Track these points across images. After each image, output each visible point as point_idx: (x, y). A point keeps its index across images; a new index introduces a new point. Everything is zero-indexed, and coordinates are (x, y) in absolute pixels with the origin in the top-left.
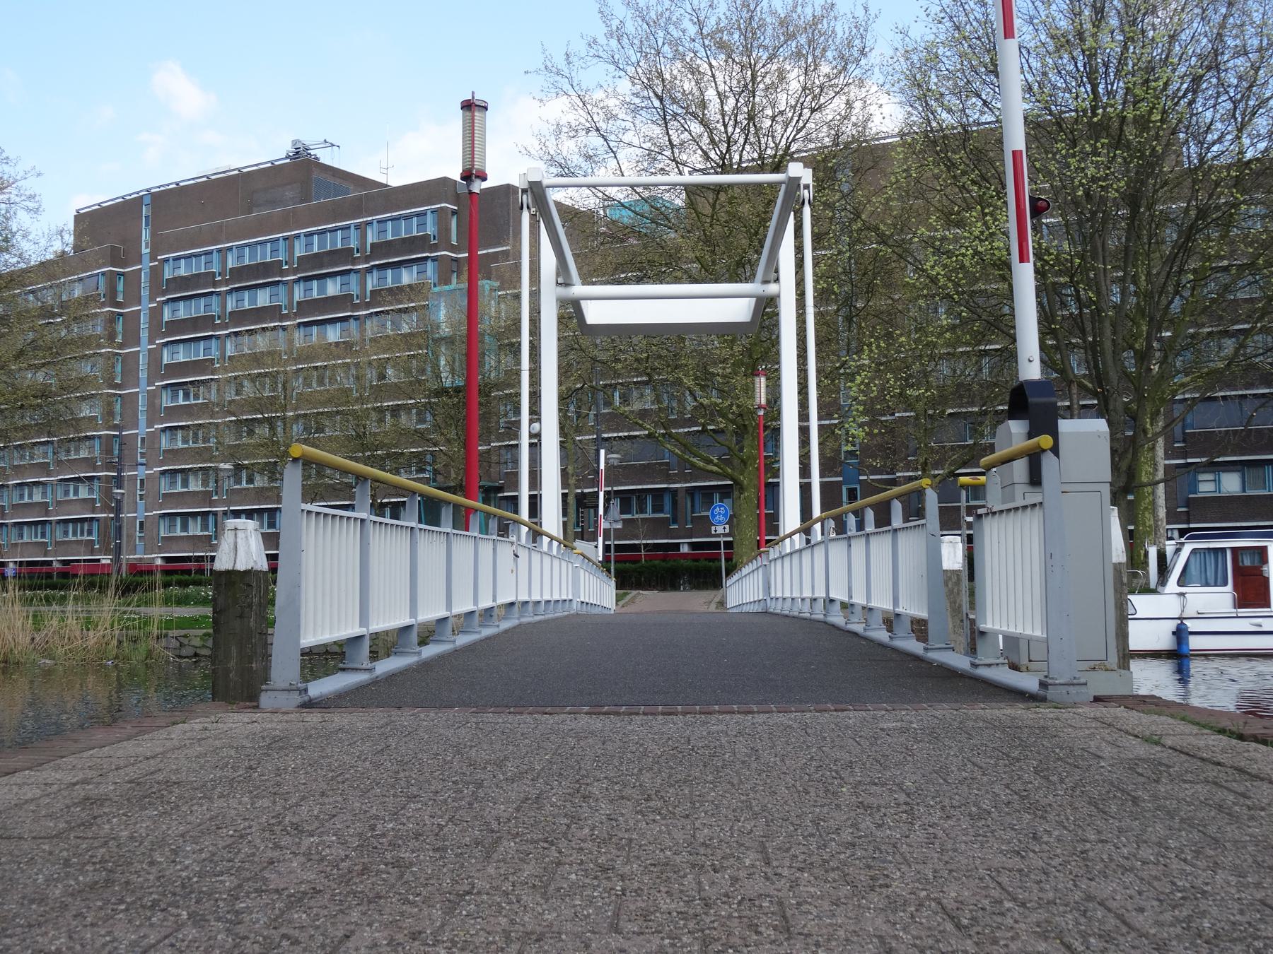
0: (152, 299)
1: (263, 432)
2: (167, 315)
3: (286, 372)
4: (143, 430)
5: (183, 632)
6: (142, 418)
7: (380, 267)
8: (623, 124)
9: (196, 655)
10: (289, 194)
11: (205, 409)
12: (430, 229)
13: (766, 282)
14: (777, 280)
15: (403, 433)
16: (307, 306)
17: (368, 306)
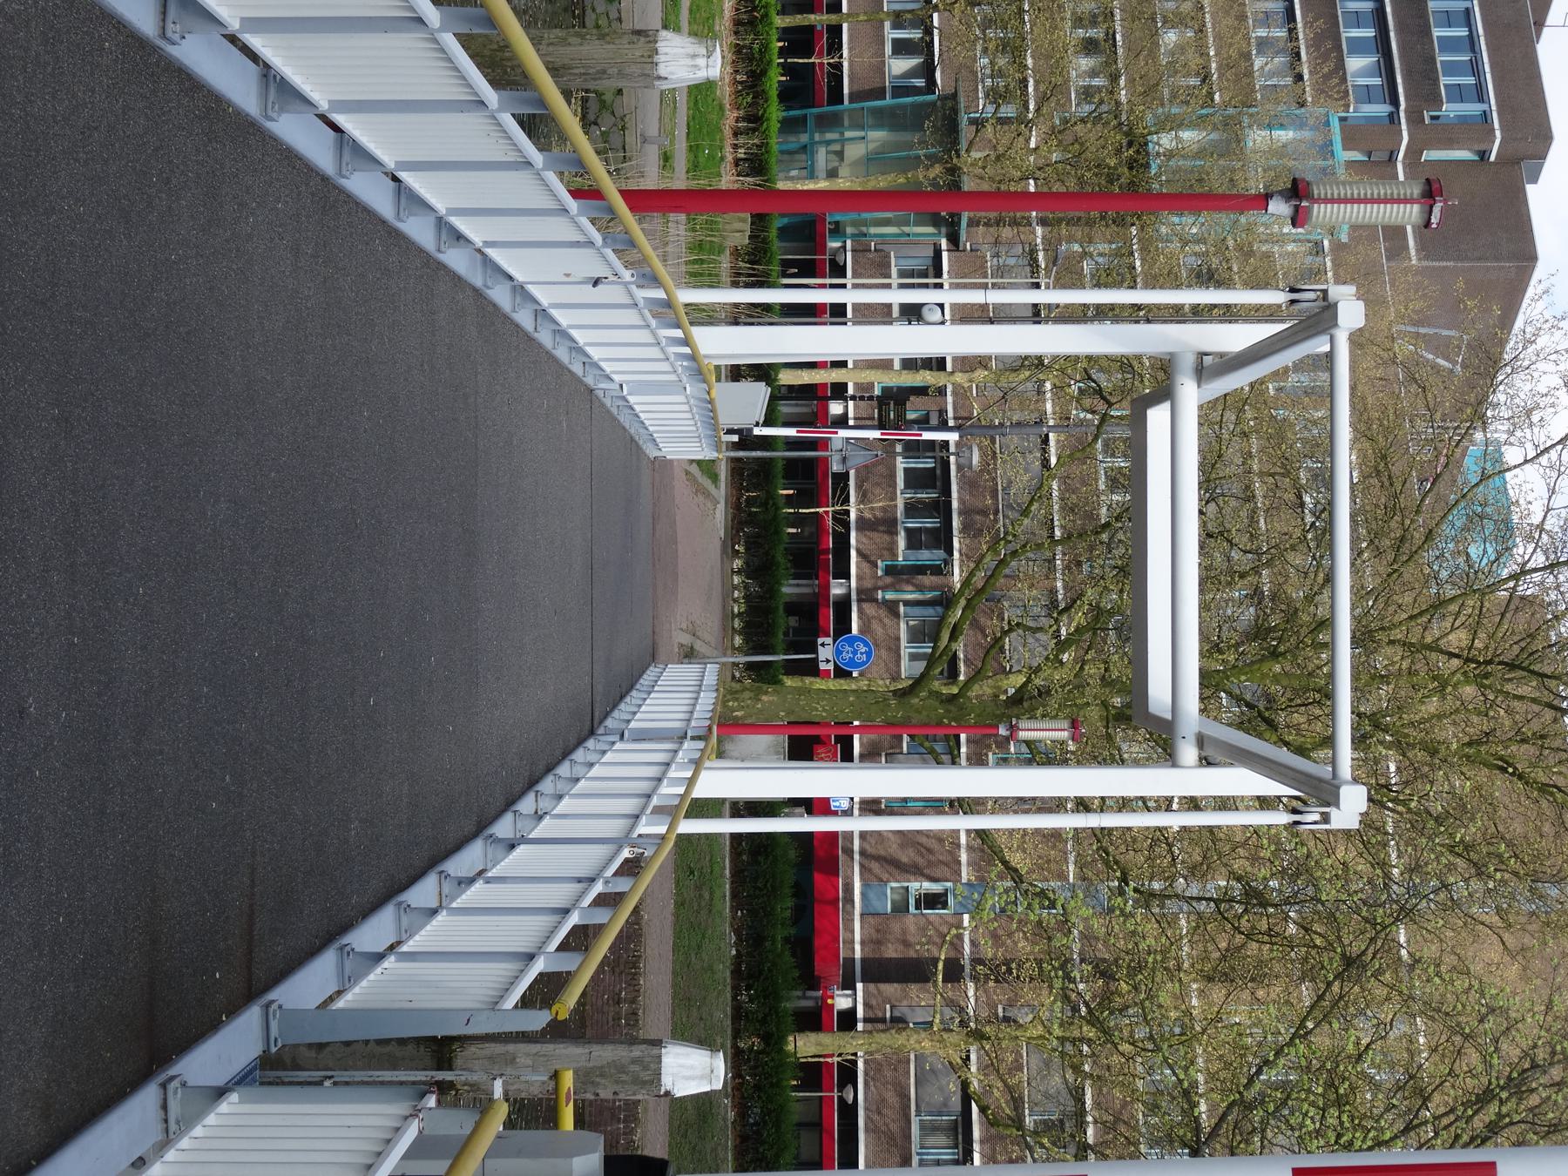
13: (1201, 741)
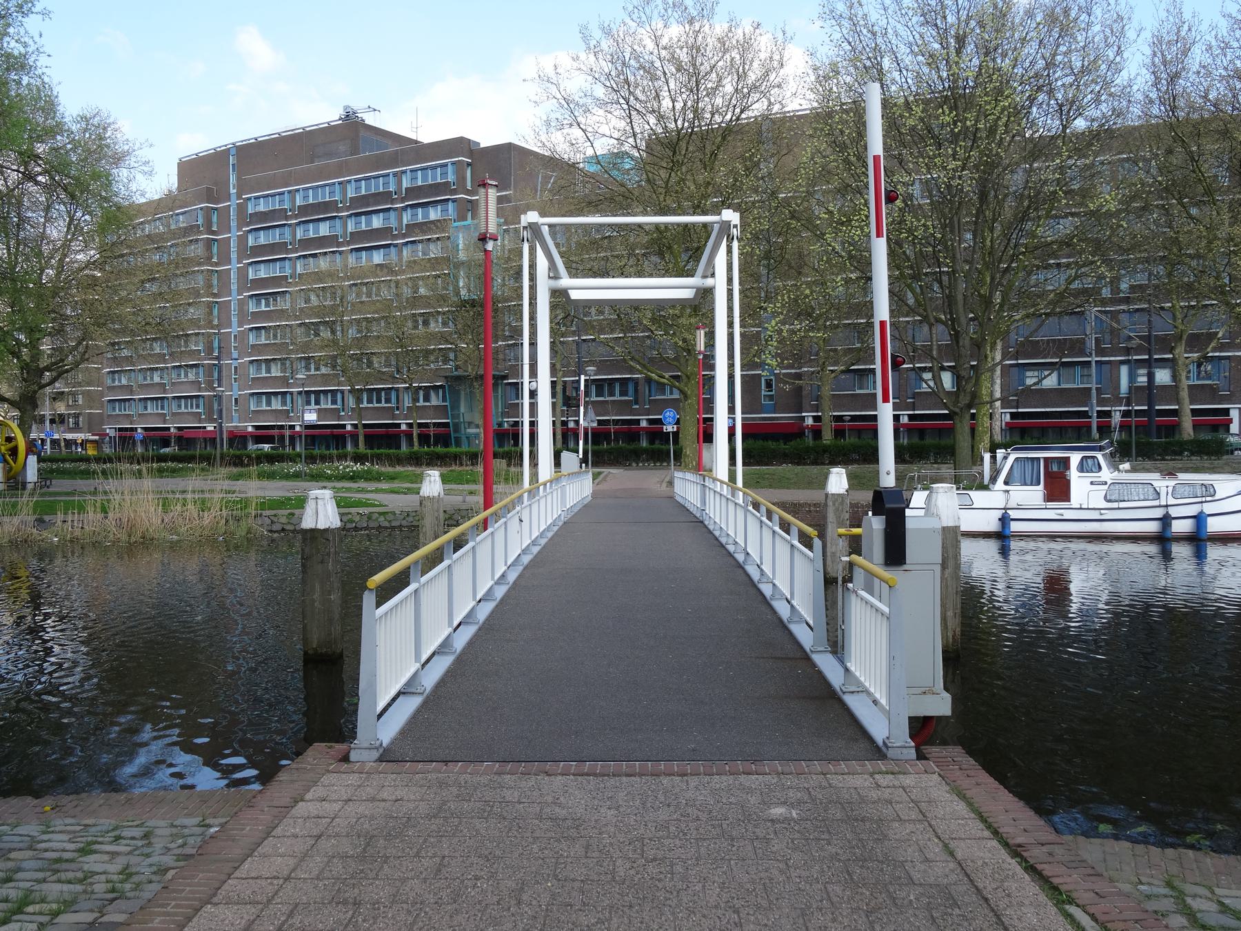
0: (239, 229)
1: (326, 334)
2: (251, 242)
3: (341, 288)
4: (235, 329)
5: (273, 512)
6: (234, 320)
7: (412, 206)
8: (598, 119)
9: (283, 530)
10: (342, 148)
11: (281, 314)
12: (451, 178)
13: (705, 277)
14: (713, 275)
15: (432, 337)
16: (357, 236)
17: (404, 236)
